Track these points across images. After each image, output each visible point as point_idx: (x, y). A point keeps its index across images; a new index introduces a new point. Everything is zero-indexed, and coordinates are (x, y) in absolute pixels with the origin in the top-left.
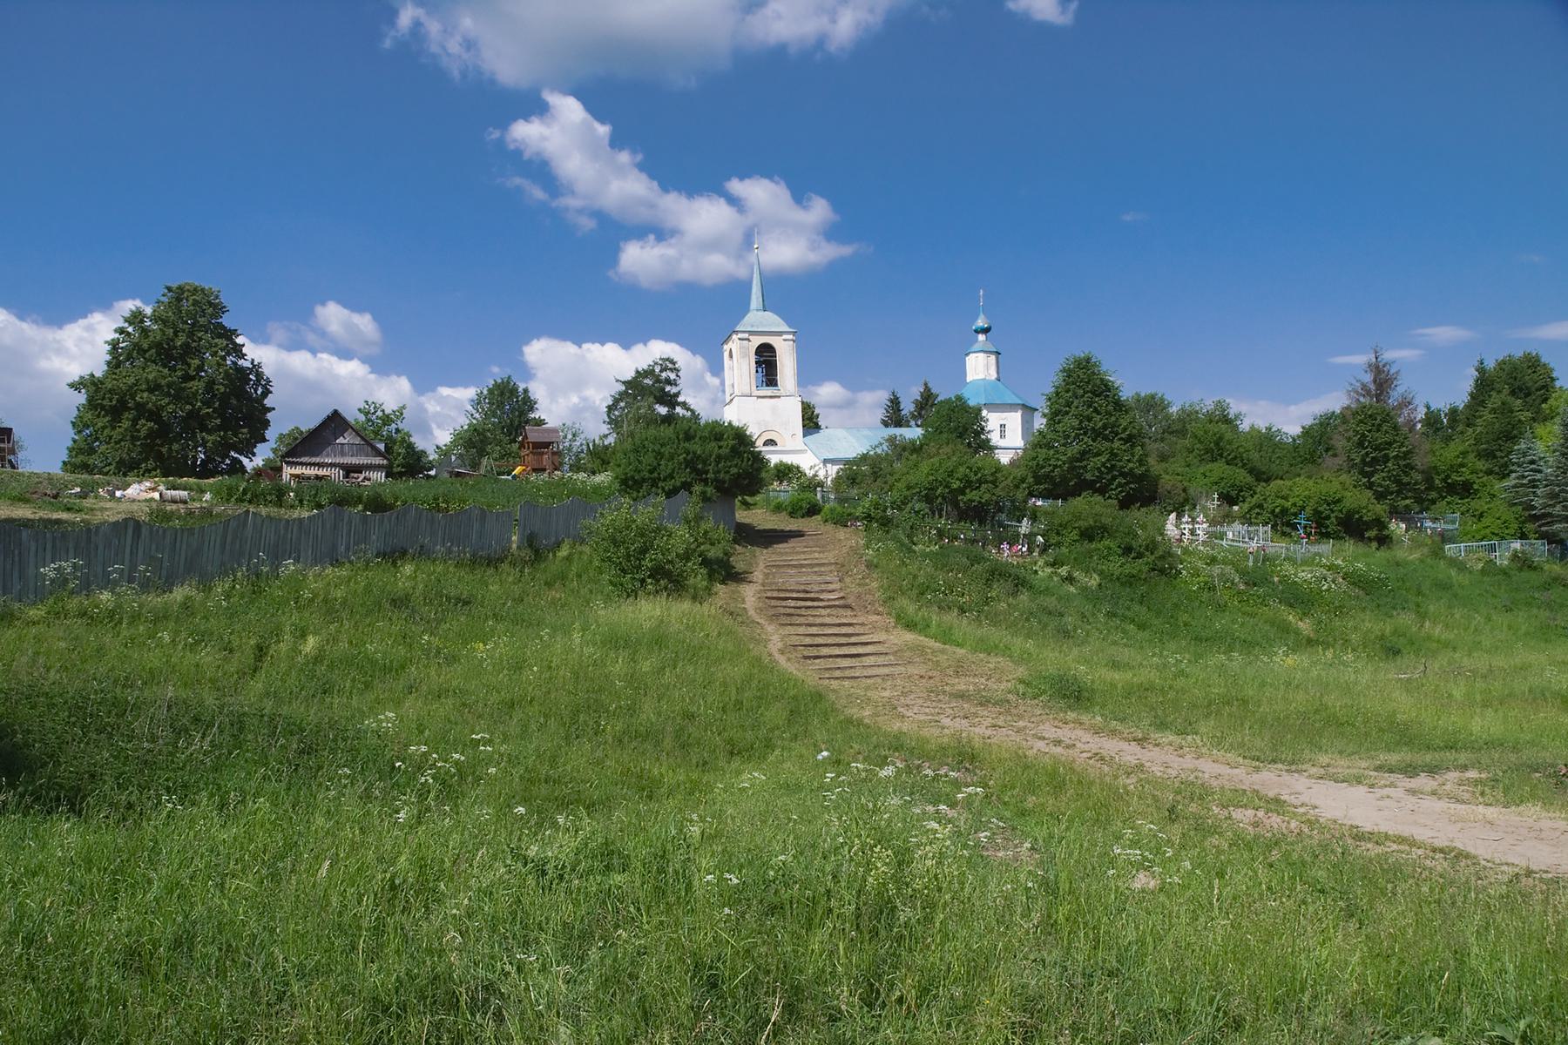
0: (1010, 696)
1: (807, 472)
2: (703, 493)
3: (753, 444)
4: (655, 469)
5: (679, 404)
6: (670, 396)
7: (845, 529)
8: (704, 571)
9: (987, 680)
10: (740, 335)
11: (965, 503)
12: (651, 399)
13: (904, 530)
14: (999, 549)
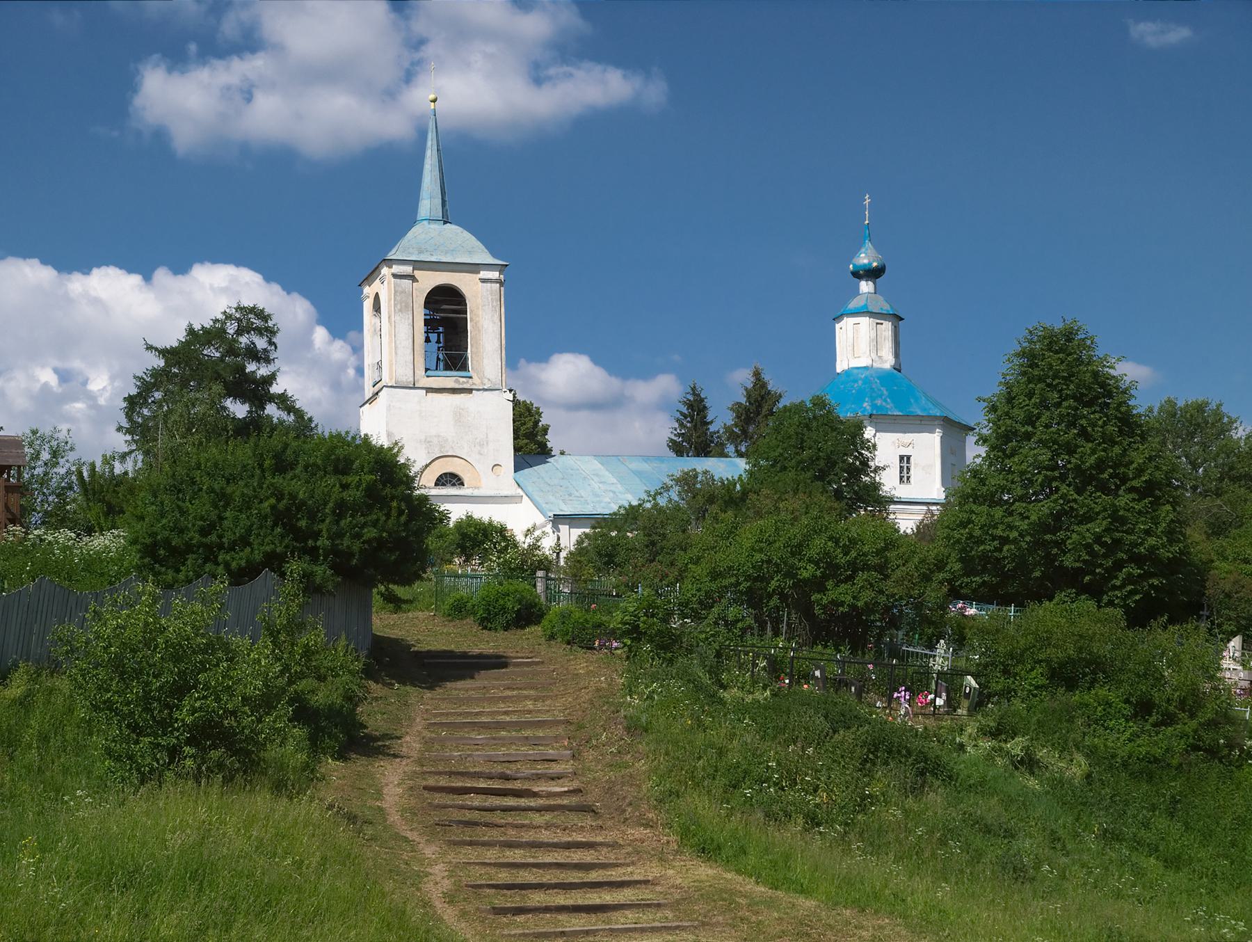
10: (397, 269)
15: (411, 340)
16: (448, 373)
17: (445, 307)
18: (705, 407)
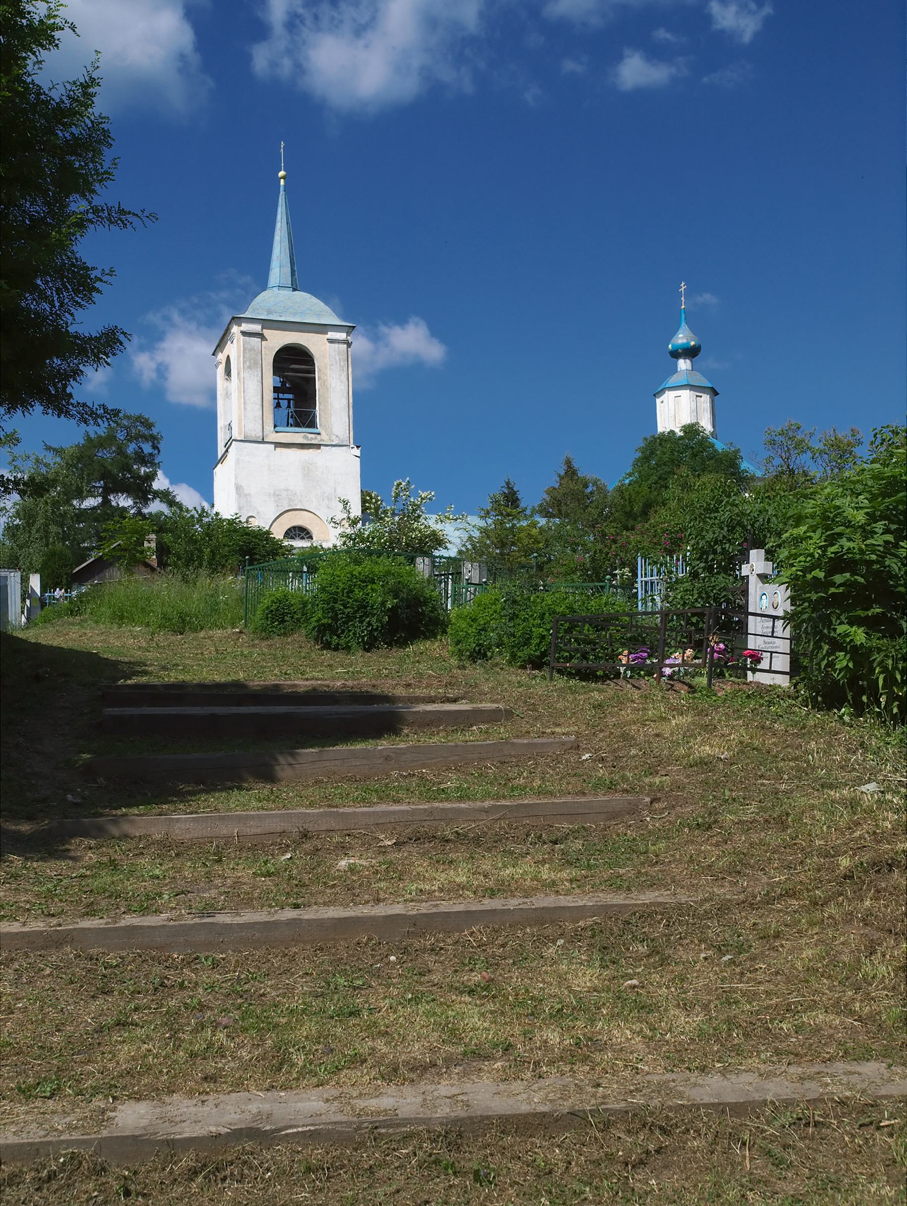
10: (245, 327)
15: (260, 397)
16: (297, 429)
17: (293, 366)
18: (517, 499)
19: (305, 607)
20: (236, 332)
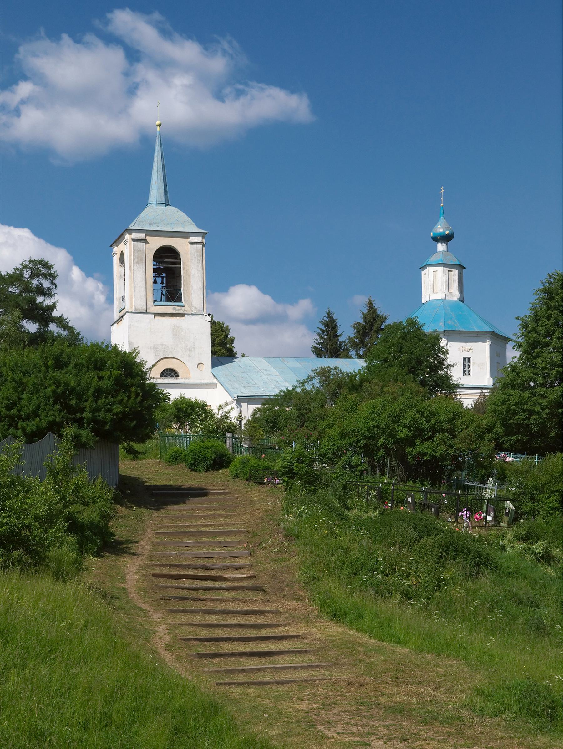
0: (464, 713)
1: (215, 411)
2: (77, 436)
3: (143, 375)
4: (14, 404)
5: (53, 320)
6: (42, 309)
7: (260, 487)
8: (71, 539)
9: (435, 689)
10: (135, 235)
11: (414, 456)
12: (17, 313)
13: (335, 490)
14: (457, 516)
15: (144, 282)
16: (169, 303)
17: (166, 260)
18: (336, 326)
19: (185, 457)
20: (128, 238)
